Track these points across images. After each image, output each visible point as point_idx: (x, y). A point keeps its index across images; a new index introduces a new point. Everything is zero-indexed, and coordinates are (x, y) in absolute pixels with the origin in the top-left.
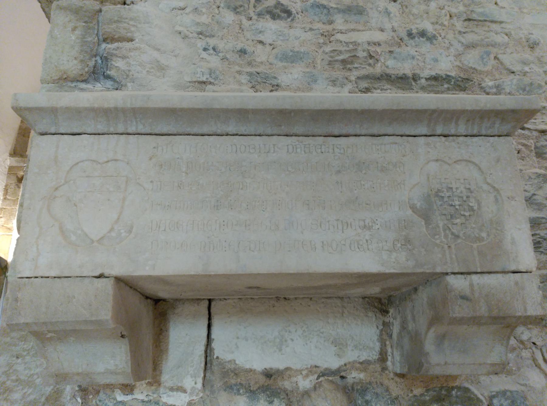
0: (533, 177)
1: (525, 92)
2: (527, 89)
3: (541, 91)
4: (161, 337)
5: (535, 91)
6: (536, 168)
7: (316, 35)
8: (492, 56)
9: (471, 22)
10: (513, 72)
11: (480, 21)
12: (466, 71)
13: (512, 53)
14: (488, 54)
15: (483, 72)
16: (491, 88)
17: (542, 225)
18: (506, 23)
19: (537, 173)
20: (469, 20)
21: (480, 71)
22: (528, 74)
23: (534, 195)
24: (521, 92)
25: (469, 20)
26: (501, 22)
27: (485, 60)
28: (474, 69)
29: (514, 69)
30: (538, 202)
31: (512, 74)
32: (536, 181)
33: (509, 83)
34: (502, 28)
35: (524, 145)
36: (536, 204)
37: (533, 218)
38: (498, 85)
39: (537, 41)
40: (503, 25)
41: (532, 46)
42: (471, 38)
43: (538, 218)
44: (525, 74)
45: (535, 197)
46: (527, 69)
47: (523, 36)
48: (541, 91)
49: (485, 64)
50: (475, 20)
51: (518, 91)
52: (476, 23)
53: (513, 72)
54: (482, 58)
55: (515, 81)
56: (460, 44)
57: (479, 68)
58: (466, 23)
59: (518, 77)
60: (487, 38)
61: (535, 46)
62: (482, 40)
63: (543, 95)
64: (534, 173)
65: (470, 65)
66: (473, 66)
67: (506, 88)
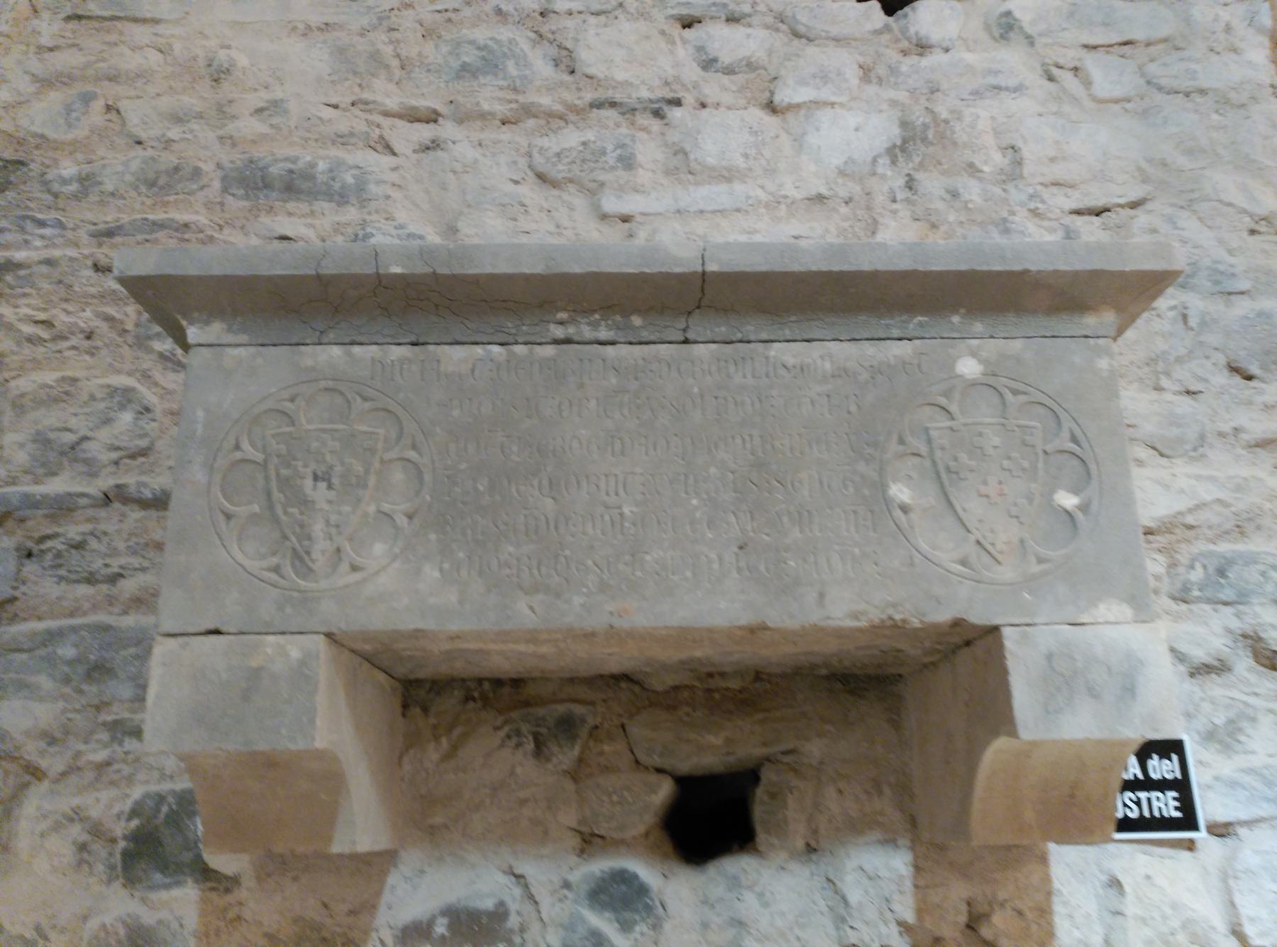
0: (99, 395)
1: (156, 189)
2: (161, 182)
3: (195, 187)
4: (727, 669)
5: (179, 186)
6: (119, 372)
7: (501, 88)
8: (98, 105)
9: (83, 22)
10: (139, 143)
11: (104, 19)
12: (21, 142)
13: (158, 95)
14: (87, 99)
15: (63, 143)
16: (65, 182)
17: (80, 512)
18: (166, 21)
19: (109, 386)
20: (79, 18)
21: (55, 141)
22: (175, 147)
23: (85, 438)
24: (143, 189)
25: (79, 18)
26: (156, 21)
27: (74, 115)
28: (42, 136)
29: (143, 136)
30: (89, 455)
31: (138, 147)
32: (102, 405)
33: (120, 168)
34: (156, 34)
35: (109, 319)
36: (86, 462)
37: (57, 495)
38: (87, 176)
39: (226, 65)
40: (160, 29)
41: (216, 76)
42: (66, 60)
43: (70, 495)
44: (168, 143)
45: (85, 445)
46: (174, 133)
47: (200, 53)
48: (195, 187)
49: (70, 125)
50: (89, 18)
51: (136, 188)
52: (95, 24)
53: (139, 143)
54: (69, 109)
55: (134, 165)
56: (27, 78)
57: (52, 135)
58: (73, 25)
59: (150, 152)
60: (104, 60)
61: (222, 76)
62: (88, 65)
63: (201, 195)
64: (103, 386)
65: (34, 129)
66: (39, 131)
67: (106, 180)
